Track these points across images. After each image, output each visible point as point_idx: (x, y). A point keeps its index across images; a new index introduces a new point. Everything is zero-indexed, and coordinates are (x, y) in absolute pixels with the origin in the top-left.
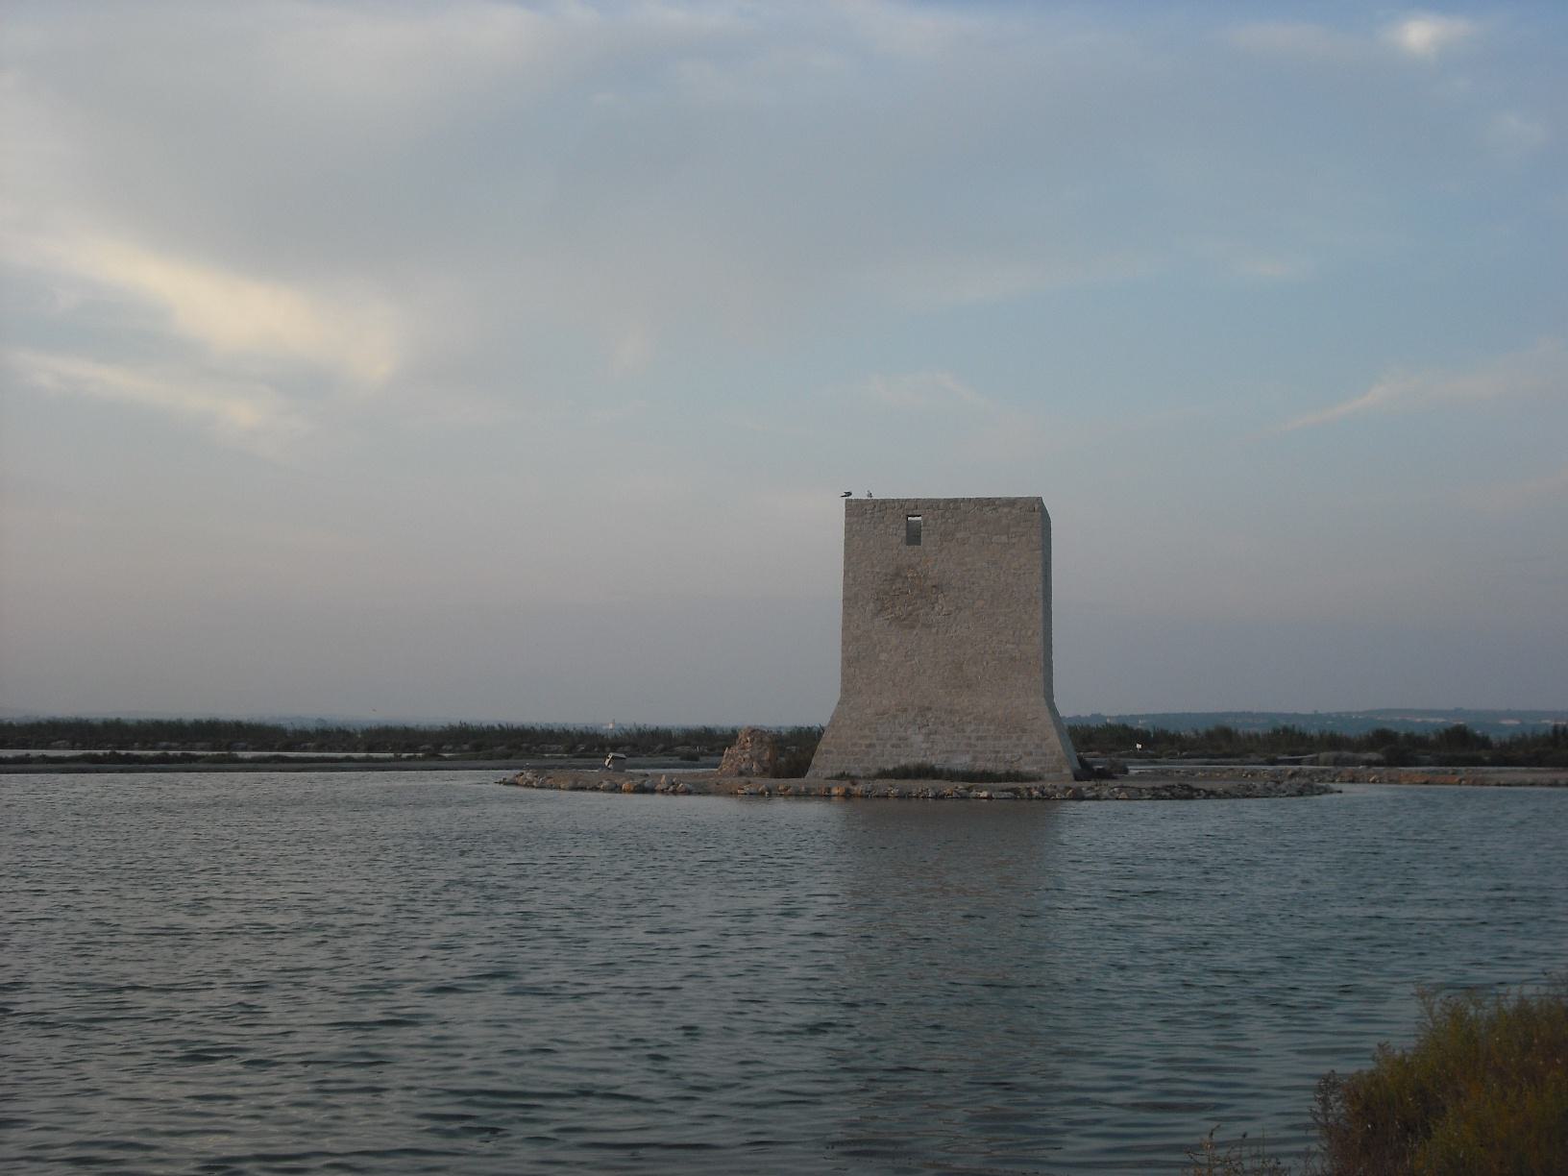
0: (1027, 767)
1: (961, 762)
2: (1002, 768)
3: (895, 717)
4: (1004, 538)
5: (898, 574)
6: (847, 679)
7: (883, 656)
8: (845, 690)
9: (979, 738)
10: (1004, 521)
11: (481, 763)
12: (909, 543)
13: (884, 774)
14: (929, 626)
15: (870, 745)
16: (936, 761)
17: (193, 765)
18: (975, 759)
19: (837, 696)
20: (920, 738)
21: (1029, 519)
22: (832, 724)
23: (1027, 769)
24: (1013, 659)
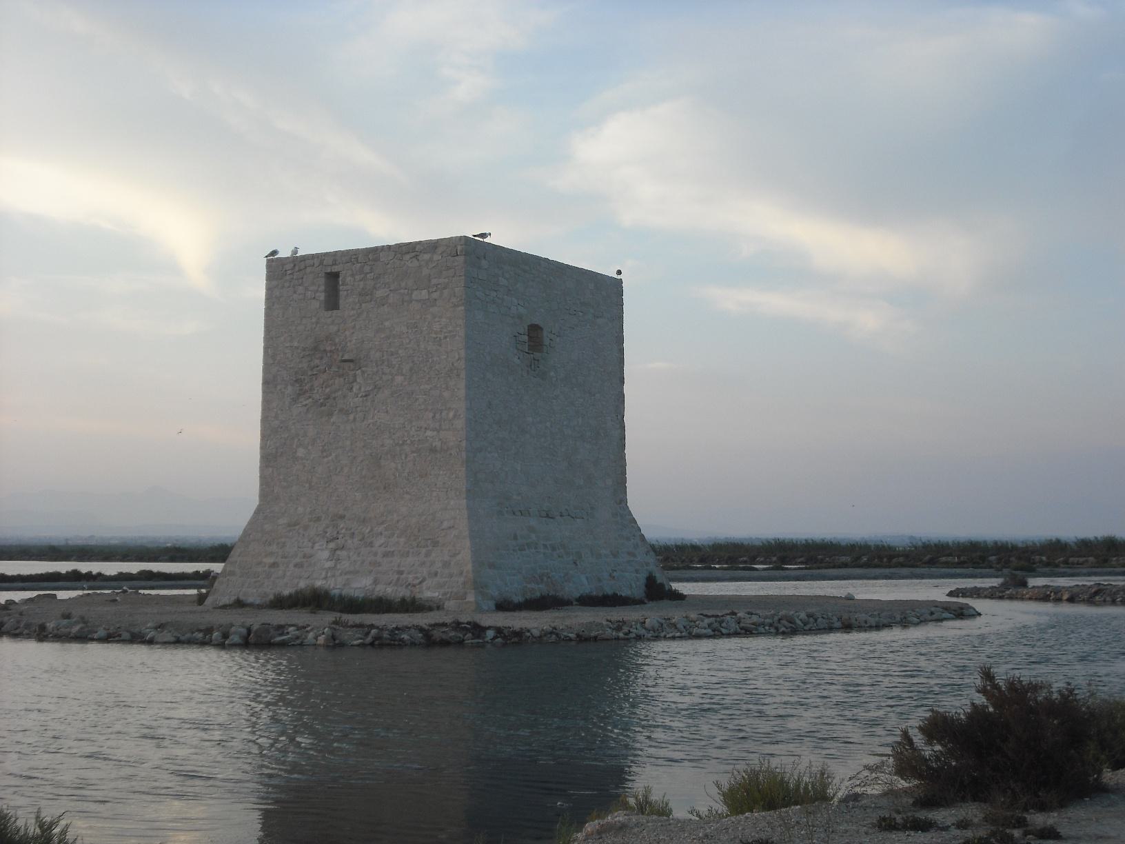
0: (428, 593)
1: (360, 586)
2: (401, 592)
3: (306, 528)
4: (424, 294)
5: (315, 349)
6: (265, 481)
7: (301, 452)
8: (264, 495)
9: (386, 555)
10: (425, 272)
11: (878, 571)
12: (328, 309)
13: (280, 603)
14: (347, 413)
15: (274, 565)
16: (335, 585)
17: (15, 585)
18: (376, 582)
19: (254, 500)
20: (326, 554)
21: (598, 299)
22: (242, 539)
23: (428, 594)
24: (433, 450)
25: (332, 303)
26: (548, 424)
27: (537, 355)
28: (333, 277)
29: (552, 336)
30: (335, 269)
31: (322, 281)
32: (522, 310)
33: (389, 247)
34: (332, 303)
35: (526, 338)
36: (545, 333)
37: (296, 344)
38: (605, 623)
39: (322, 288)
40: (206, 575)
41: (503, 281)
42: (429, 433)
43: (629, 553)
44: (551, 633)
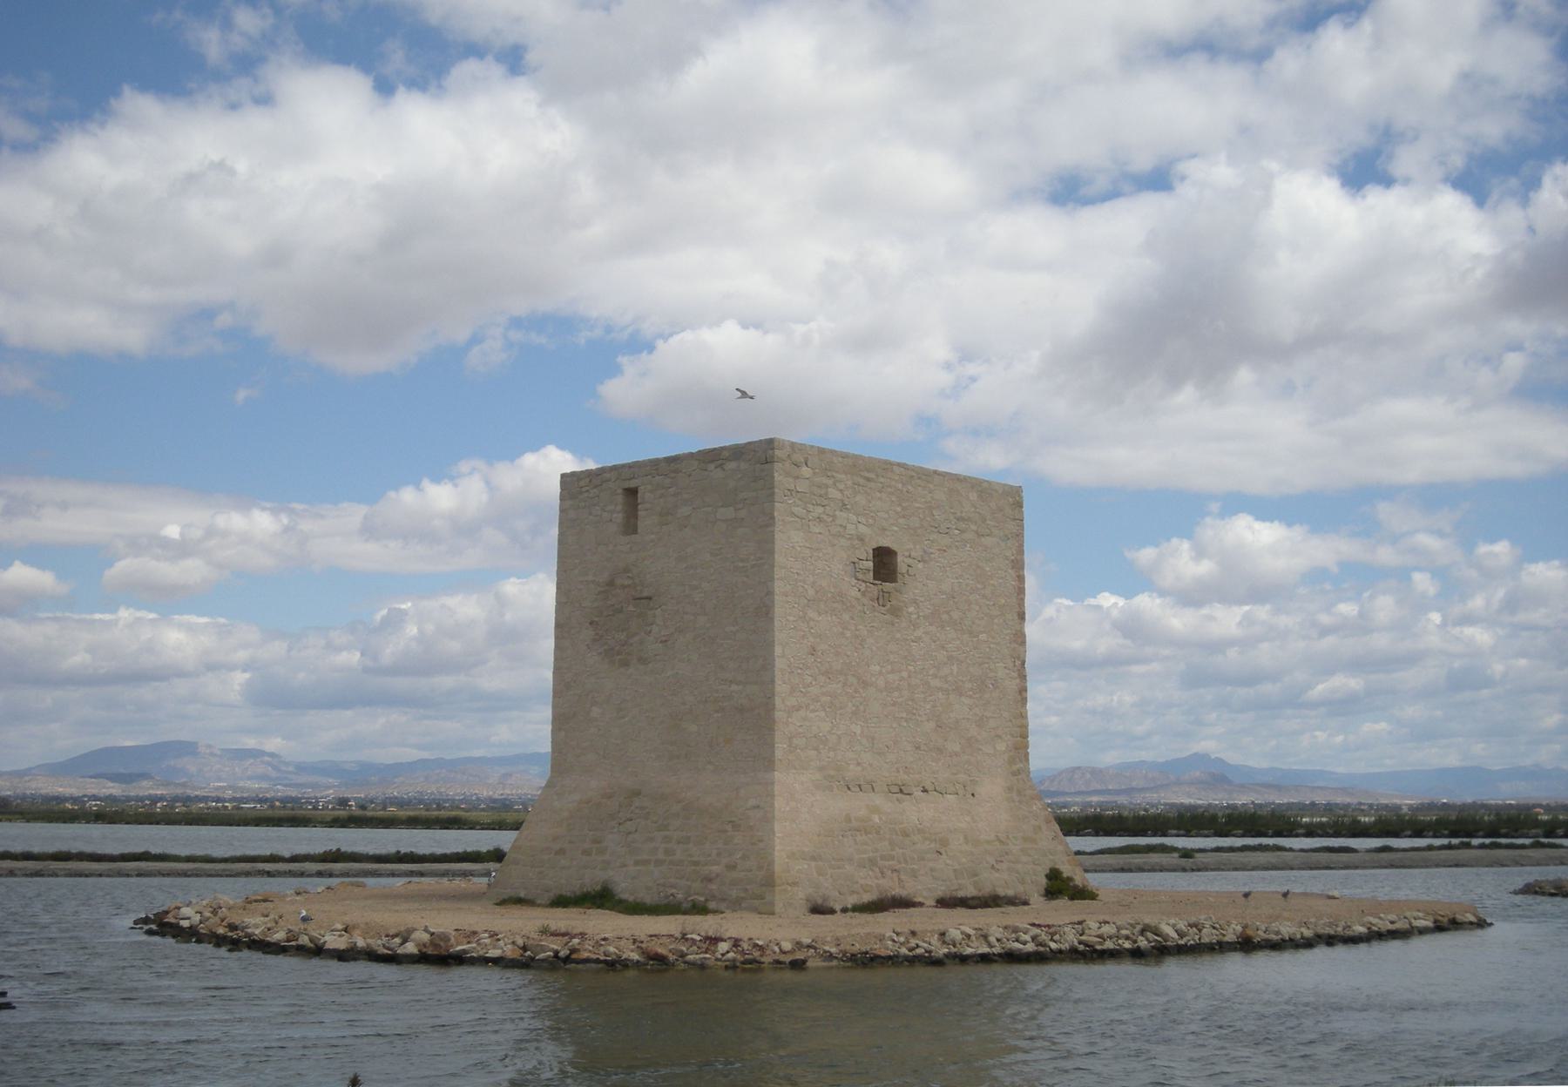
4: (728, 513)
5: (611, 583)
7: (596, 712)
25: (630, 527)
26: (905, 674)
27: (888, 586)
28: (632, 493)
29: (910, 561)
30: (632, 484)
31: (620, 498)
32: (863, 529)
33: (691, 454)
34: (630, 527)
35: (871, 564)
36: (900, 559)
37: (590, 578)
38: (889, 934)
39: (619, 508)
40: (498, 856)
41: (833, 493)
42: (734, 687)
43: (1025, 839)
44: (809, 947)
